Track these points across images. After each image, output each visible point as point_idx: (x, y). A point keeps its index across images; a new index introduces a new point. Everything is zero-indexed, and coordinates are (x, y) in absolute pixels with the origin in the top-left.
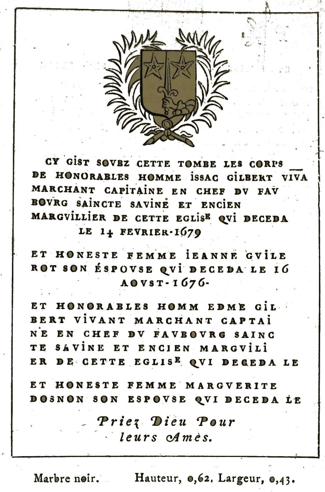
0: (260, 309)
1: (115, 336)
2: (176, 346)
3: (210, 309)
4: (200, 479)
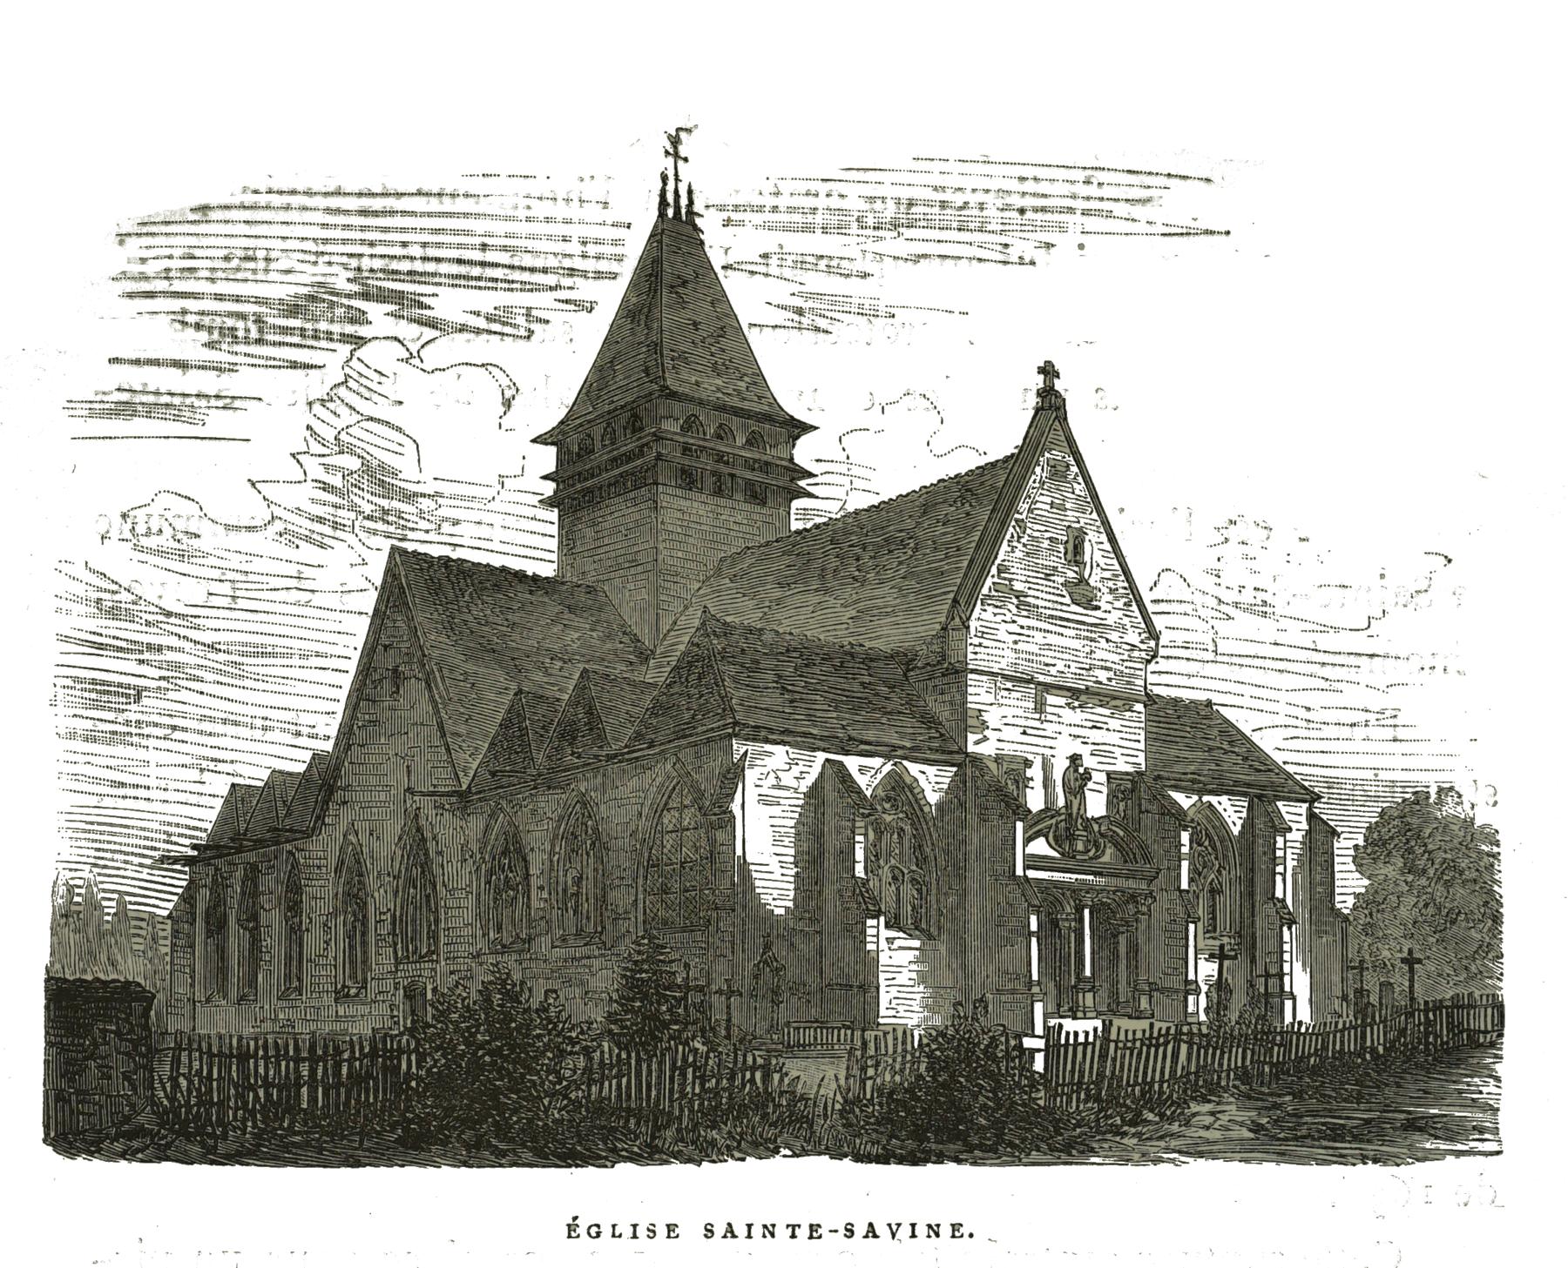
0: (598, 1235)
1: (793, 1236)
2: (811, 1226)
3: (570, 1236)
4: (730, 1232)
